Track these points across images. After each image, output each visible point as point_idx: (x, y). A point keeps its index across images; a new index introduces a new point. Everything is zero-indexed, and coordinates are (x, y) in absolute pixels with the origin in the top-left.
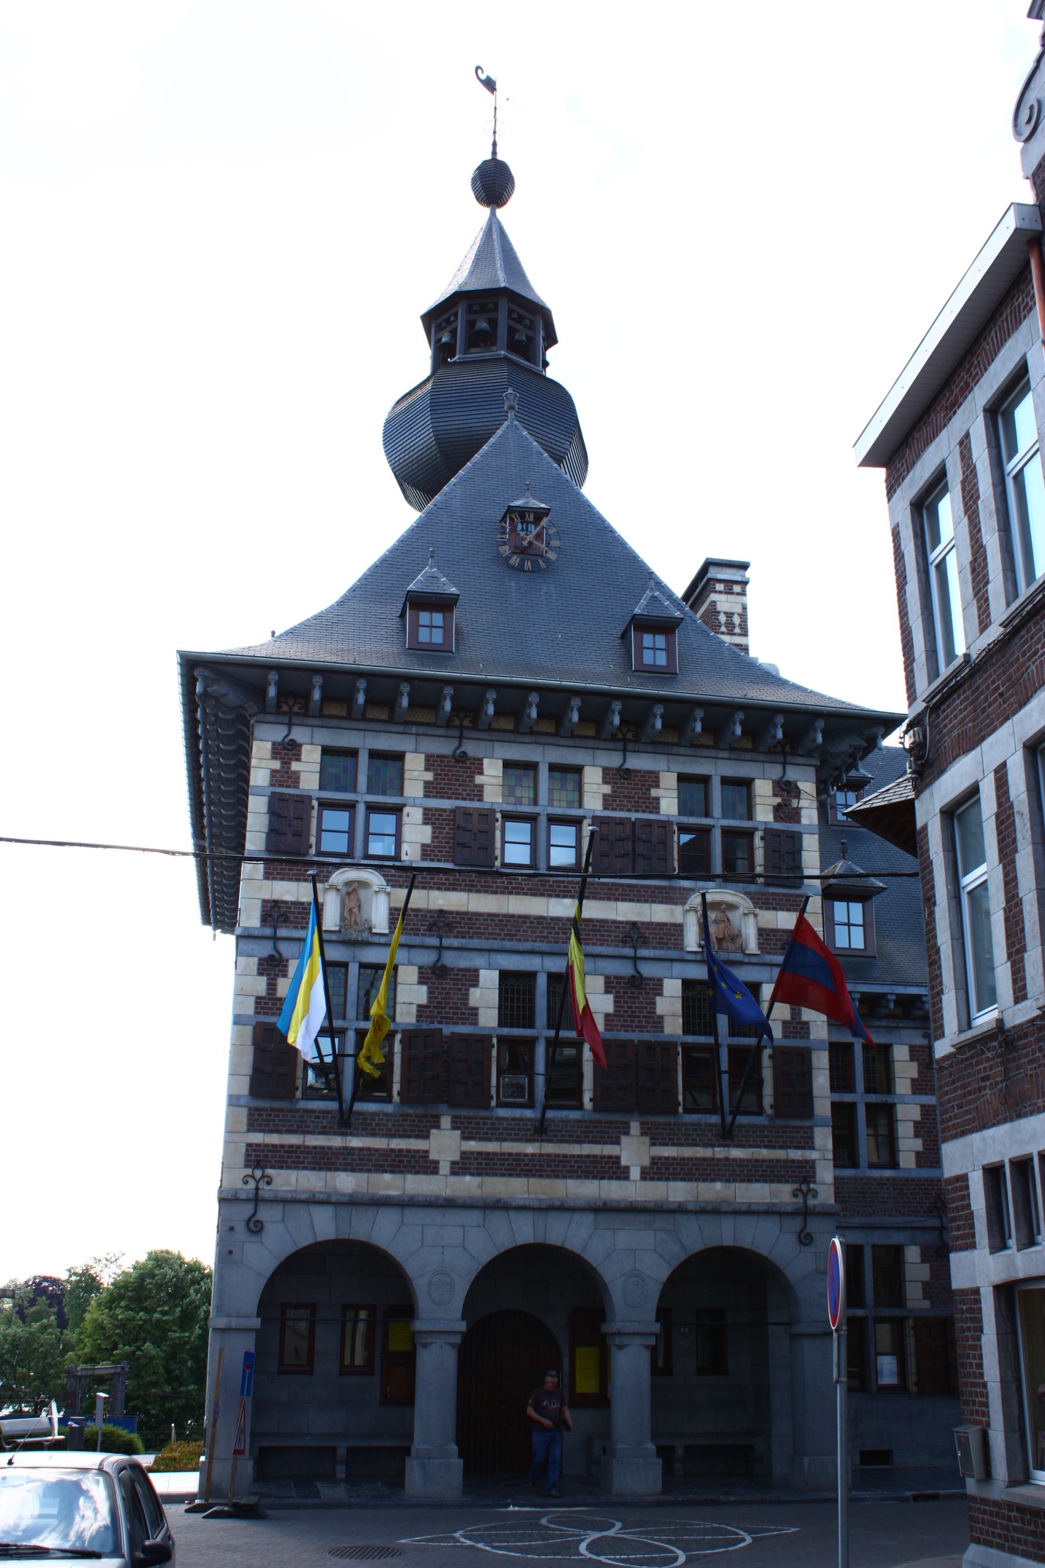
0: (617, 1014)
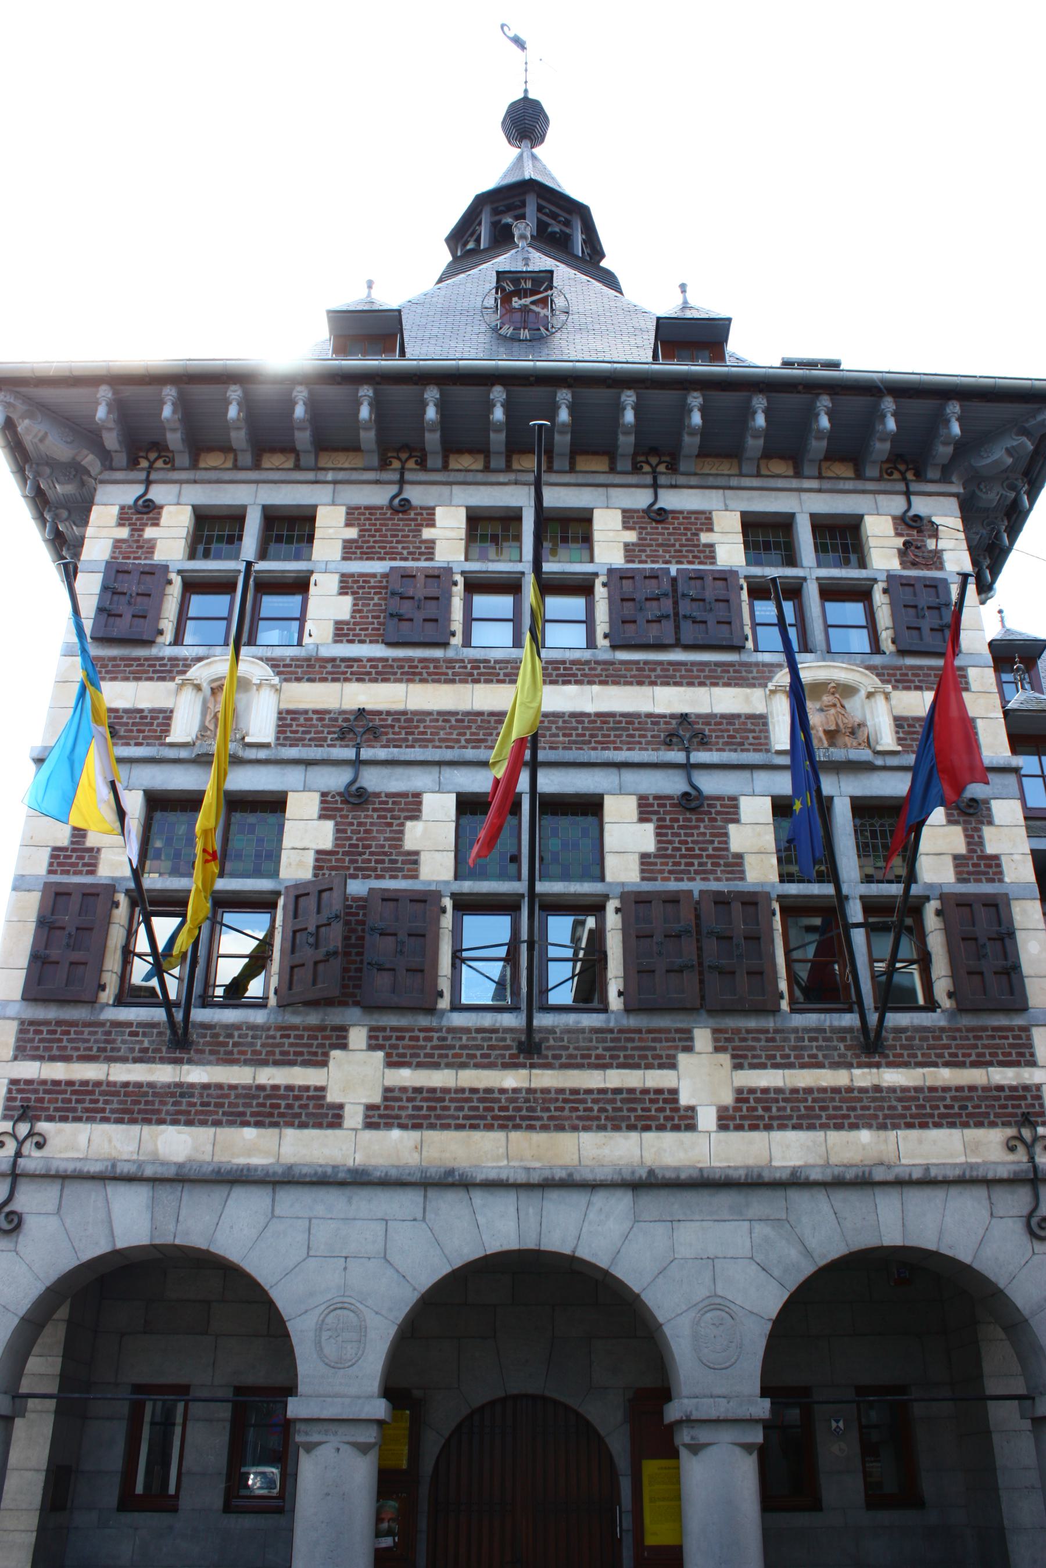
0: (661, 852)
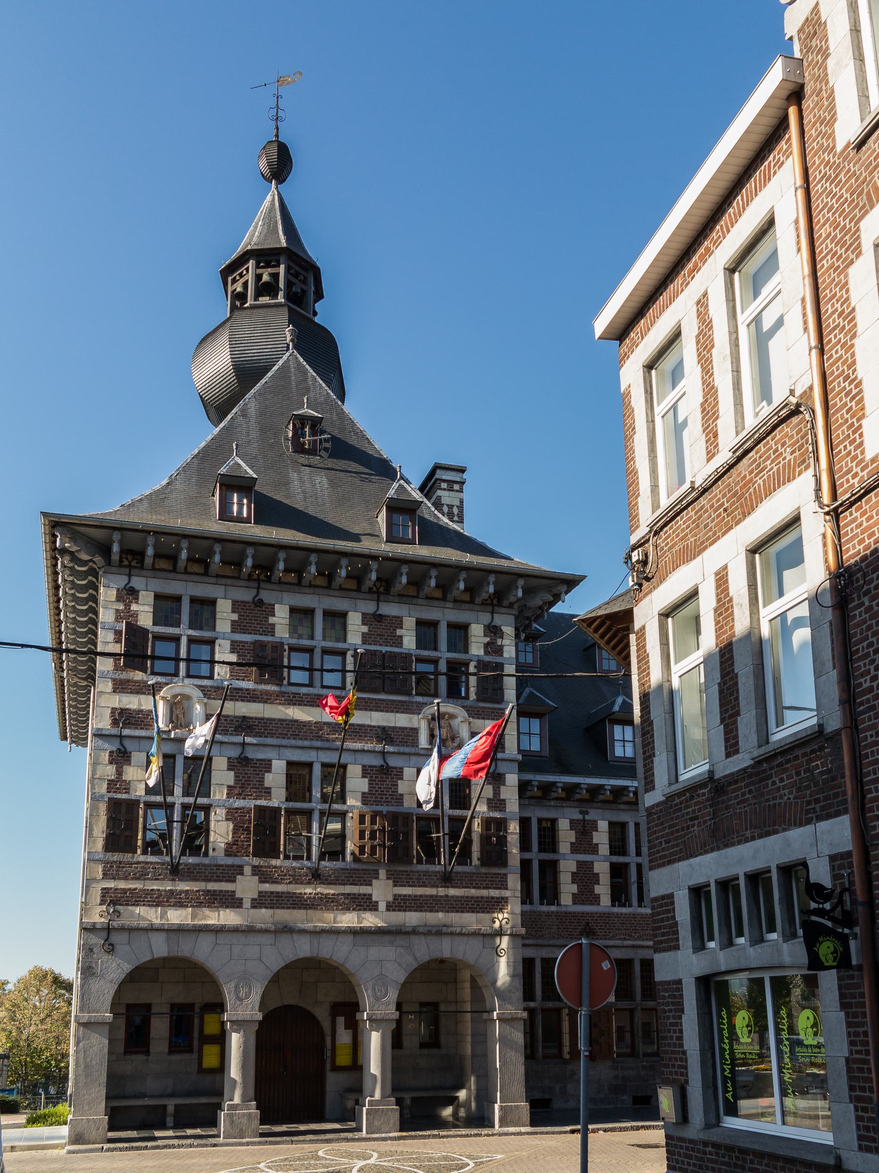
0: (370, 793)
